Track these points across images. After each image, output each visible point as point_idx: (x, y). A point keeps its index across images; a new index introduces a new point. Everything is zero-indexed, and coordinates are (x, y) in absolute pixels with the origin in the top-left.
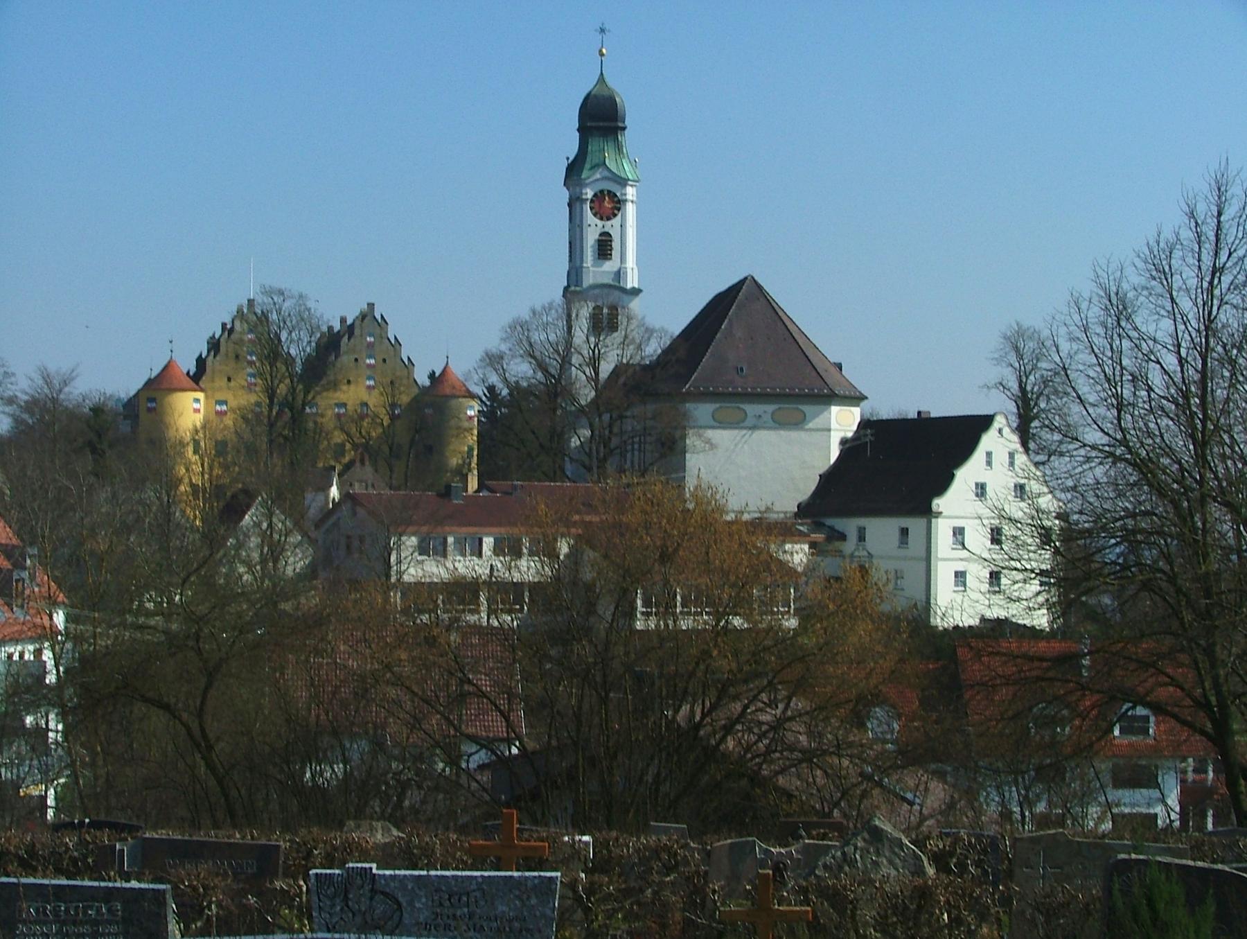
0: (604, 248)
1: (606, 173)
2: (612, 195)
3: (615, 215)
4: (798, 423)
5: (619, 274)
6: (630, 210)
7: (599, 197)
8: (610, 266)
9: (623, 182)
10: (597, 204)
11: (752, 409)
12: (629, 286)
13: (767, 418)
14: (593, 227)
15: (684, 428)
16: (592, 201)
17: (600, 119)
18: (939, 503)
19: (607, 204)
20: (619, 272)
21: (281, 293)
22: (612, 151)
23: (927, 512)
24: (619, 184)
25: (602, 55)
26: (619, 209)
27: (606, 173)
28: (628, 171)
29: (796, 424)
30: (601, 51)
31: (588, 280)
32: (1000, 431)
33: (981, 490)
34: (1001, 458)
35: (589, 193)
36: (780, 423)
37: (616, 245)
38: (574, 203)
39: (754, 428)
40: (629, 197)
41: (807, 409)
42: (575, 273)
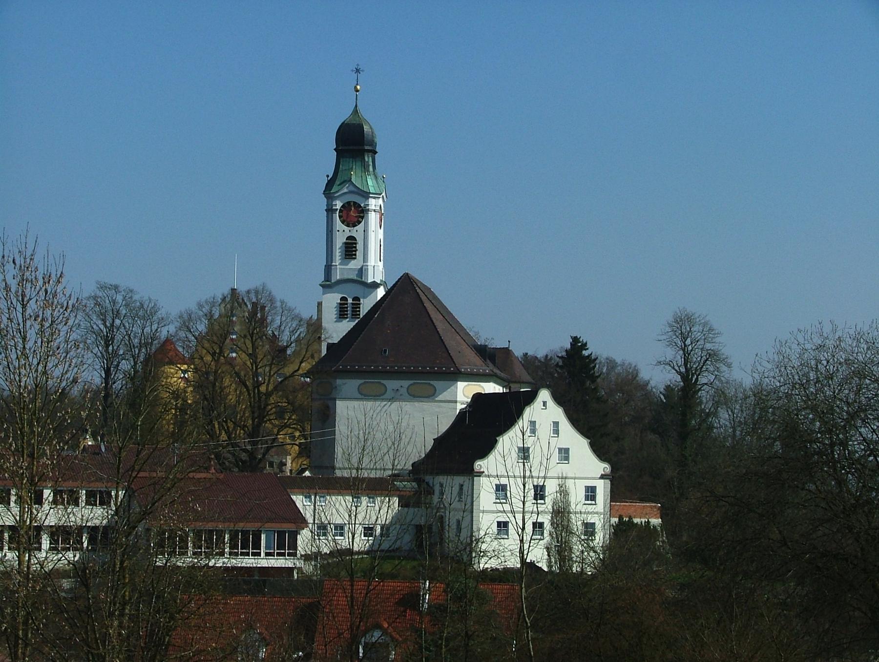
0: (350, 249)
1: (352, 188)
2: (357, 206)
3: (360, 223)
4: (430, 395)
5: (362, 271)
6: (373, 218)
7: (346, 207)
8: (354, 264)
9: (366, 195)
10: (345, 212)
11: (391, 384)
12: (370, 280)
13: (404, 391)
14: (342, 232)
15: (335, 399)
16: (341, 211)
17: (353, 143)
18: (480, 465)
19: (353, 213)
20: (362, 268)
21: (116, 288)
22: (359, 171)
23: (471, 473)
24: (363, 196)
25: (357, 91)
26: (362, 218)
27: (352, 188)
28: (371, 184)
29: (428, 397)
30: (355, 87)
31: (337, 276)
32: (545, 404)
33: (524, 453)
34: (545, 430)
35: (338, 204)
36: (414, 395)
37: (360, 246)
38: (330, 210)
39: (392, 400)
40: (372, 207)
41: (437, 384)
42: (328, 269)
